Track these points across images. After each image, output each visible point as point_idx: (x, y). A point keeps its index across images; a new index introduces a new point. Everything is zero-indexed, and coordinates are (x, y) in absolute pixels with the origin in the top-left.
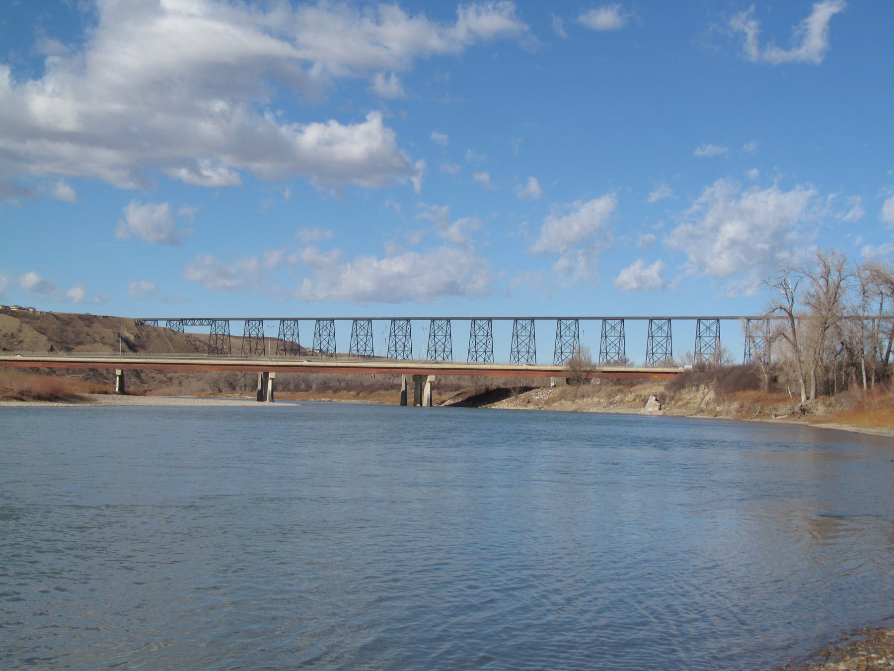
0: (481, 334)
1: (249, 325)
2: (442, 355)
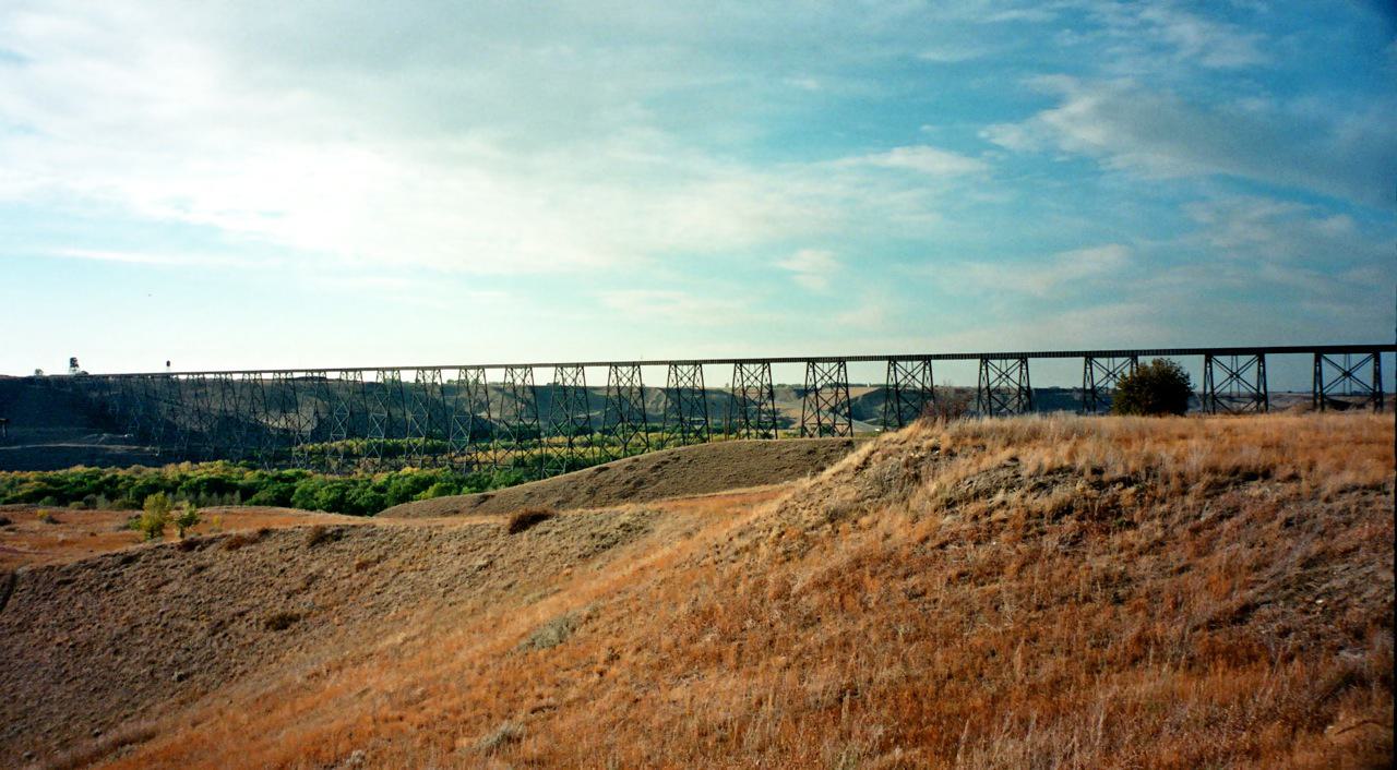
1: (814, 371)
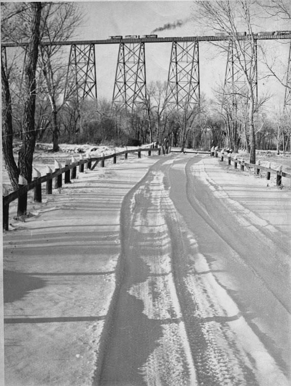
0: (131, 61)
2: (133, 87)
